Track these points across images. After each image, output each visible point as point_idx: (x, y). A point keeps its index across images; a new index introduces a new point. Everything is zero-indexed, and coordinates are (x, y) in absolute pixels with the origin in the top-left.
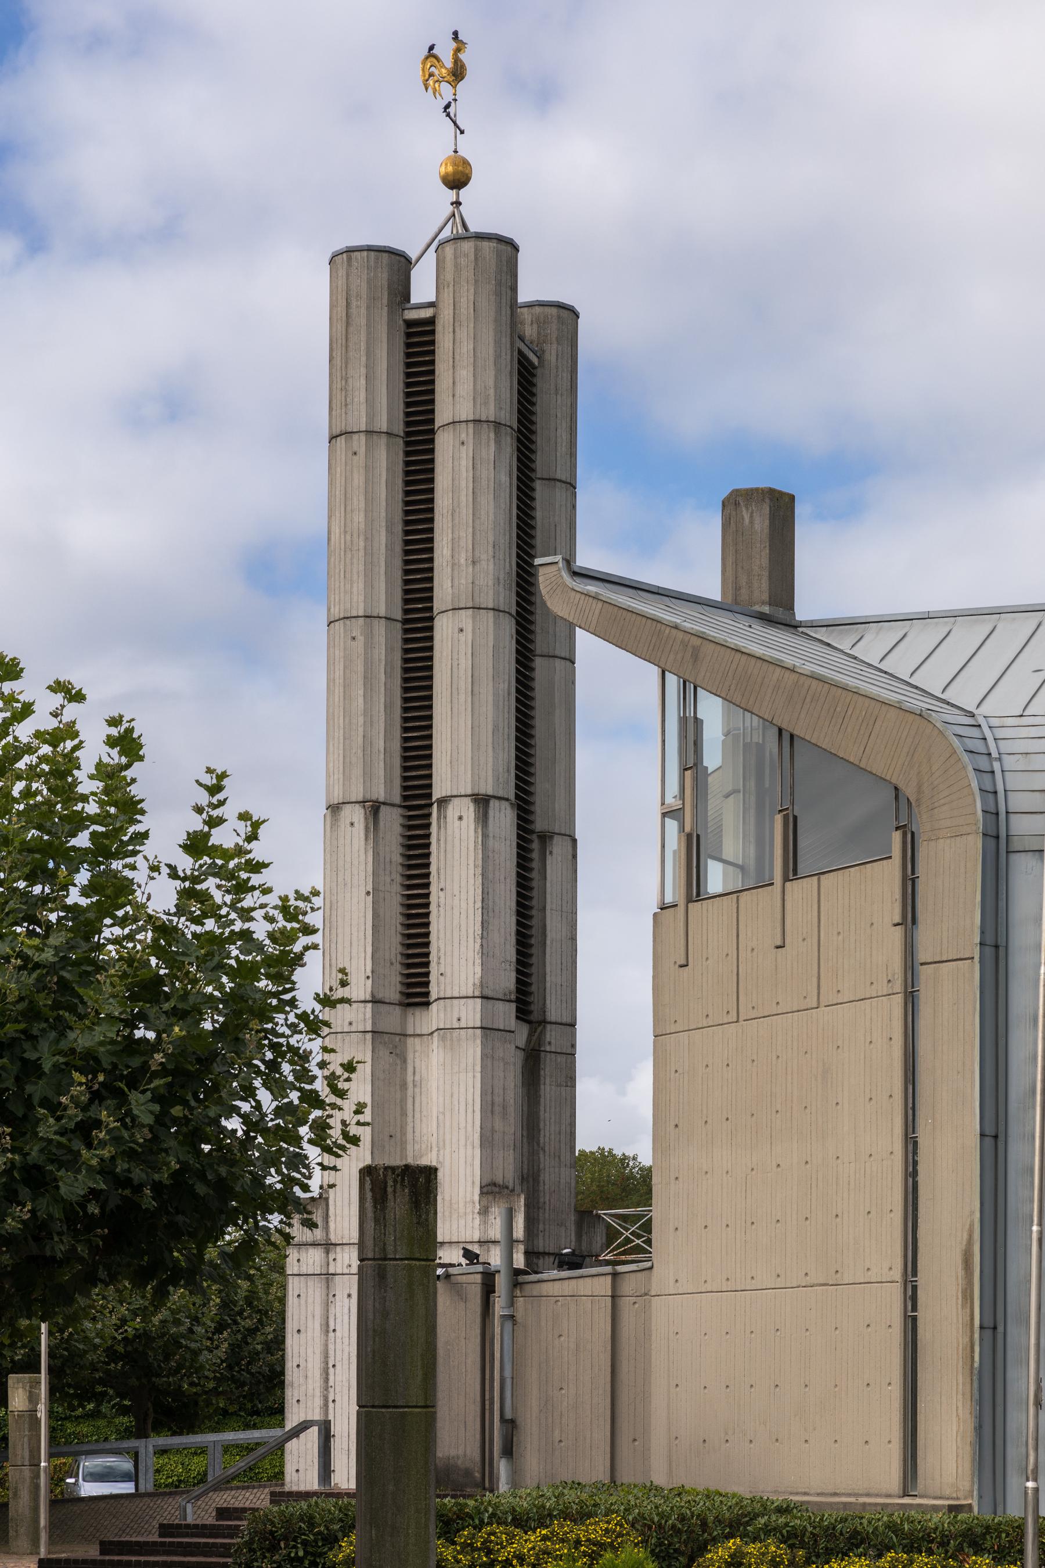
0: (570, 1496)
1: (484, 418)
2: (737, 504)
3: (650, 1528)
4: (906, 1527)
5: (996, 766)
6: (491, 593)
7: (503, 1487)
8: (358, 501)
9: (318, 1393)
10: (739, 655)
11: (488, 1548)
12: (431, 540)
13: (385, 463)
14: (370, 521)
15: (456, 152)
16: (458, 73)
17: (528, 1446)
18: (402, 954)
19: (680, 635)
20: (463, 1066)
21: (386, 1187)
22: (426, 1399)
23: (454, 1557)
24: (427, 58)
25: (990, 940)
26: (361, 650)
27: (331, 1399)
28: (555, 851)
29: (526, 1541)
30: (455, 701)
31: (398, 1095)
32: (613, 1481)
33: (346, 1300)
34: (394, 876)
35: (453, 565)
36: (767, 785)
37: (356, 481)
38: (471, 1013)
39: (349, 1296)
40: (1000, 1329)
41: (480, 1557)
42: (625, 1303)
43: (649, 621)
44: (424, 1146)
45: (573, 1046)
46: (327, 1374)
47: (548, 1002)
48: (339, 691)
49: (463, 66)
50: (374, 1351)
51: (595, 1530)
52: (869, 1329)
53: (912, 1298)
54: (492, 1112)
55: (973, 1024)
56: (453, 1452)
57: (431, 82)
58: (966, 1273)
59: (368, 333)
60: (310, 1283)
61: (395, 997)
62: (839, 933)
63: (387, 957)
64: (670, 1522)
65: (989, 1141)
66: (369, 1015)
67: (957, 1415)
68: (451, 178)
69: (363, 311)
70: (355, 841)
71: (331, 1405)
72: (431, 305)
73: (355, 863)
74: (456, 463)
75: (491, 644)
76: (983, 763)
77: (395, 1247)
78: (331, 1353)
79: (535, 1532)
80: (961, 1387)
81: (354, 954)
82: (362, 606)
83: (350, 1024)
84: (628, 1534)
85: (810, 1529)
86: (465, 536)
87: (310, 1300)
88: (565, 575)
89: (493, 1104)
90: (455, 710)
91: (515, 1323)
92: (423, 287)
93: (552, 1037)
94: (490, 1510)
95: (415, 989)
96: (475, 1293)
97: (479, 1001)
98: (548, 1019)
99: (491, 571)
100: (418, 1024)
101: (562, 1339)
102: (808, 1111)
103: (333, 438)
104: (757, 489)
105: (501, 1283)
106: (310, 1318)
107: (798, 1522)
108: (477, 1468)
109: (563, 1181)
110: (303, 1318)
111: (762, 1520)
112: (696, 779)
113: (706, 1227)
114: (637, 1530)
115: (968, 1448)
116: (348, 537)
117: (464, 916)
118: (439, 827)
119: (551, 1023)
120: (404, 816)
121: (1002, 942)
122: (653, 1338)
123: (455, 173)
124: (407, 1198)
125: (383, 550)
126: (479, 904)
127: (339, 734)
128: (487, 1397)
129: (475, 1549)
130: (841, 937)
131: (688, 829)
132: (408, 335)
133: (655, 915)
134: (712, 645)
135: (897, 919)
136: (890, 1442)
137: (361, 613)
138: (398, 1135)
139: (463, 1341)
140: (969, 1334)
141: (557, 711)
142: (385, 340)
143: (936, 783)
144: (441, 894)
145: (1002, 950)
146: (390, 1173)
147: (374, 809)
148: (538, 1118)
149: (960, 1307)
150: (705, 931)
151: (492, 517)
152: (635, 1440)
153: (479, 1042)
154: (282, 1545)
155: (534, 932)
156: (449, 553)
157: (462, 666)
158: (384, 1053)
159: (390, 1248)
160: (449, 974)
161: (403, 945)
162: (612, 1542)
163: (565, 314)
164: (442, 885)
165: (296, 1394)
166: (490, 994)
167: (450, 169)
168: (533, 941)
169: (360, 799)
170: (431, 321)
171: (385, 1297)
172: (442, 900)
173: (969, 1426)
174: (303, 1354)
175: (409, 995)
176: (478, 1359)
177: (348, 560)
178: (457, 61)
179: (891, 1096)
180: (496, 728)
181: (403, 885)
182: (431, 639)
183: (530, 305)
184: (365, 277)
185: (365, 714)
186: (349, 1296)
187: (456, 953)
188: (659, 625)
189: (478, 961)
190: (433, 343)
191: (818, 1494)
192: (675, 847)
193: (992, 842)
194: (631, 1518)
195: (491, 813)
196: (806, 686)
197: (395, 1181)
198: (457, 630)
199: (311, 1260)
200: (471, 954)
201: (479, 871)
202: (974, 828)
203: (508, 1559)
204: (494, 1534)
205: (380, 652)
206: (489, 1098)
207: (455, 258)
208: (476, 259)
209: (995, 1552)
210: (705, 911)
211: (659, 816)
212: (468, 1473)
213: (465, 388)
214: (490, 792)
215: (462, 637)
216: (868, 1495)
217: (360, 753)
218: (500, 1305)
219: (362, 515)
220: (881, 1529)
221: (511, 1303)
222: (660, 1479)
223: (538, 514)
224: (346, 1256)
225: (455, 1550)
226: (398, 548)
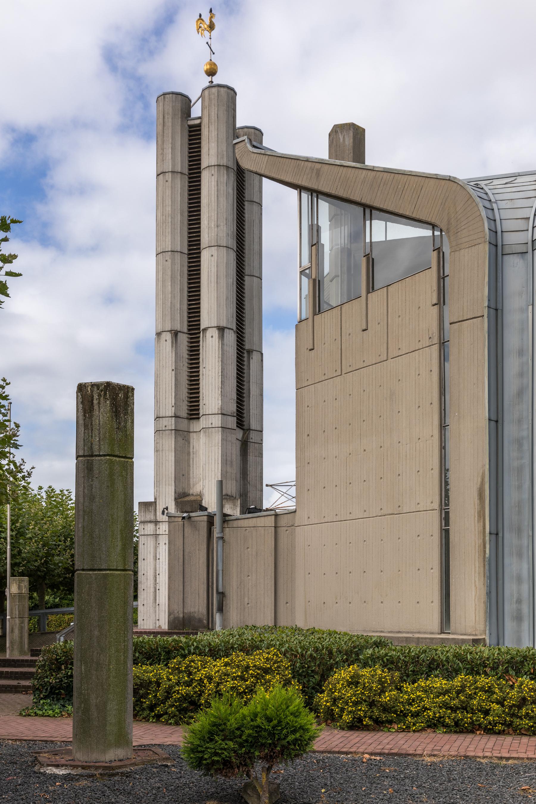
0: (248, 635)
1: (221, 164)
2: (336, 132)
3: (296, 656)
4: (469, 657)
5: (495, 206)
6: (225, 239)
7: (218, 628)
8: (168, 202)
9: (152, 586)
10: (342, 168)
11: (189, 671)
12: (200, 219)
13: (180, 185)
14: (173, 210)
15: (211, 60)
16: (211, 27)
17: (231, 606)
18: (188, 397)
19: (310, 164)
20: (213, 444)
21: (92, 400)
22: (125, 565)
23: (167, 677)
24: (199, 20)
25: (493, 306)
26: (170, 266)
27: (157, 589)
28: (254, 358)
29: (214, 666)
30: (210, 286)
31: (186, 458)
32: (275, 626)
33: (164, 546)
34: (184, 363)
35: (209, 227)
36: (352, 272)
37: (167, 193)
38: (217, 421)
39: (165, 544)
40: (500, 535)
41: (183, 678)
42: (281, 530)
43: (293, 160)
44: (197, 480)
45: (262, 440)
46: (156, 578)
47: (251, 421)
48: (160, 284)
49: (214, 24)
50: (83, 527)
51: (258, 659)
52: (419, 538)
53: (446, 518)
54: (226, 464)
55: (483, 355)
56: (192, 610)
57: (200, 30)
58: (480, 501)
59: (172, 129)
60: (149, 539)
61: (185, 415)
62: (399, 316)
63: (181, 398)
64: (309, 652)
65: (493, 423)
66: (173, 422)
67: (475, 586)
68: (209, 71)
69: (170, 120)
70: (167, 347)
71: (157, 591)
72: (200, 118)
73: (167, 357)
74: (210, 184)
75: (225, 262)
76: (488, 205)
77: (99, 446)
78: (158, 569)
79: (220, 659)
80: (477, 569)
81: (167, 396)
82: (170, 246)
83: (166, 426)
84: (281, 661)
85: (402, 658)
86: (214, 215)
87: (149, 546)
88: (249, 146)
89: (226, 460)
90: (210, 290)
91: (224, 541)
92: (196, 111)
93: (253, 436)
94: (195, 644)
95: (194, 412)
96: (204, 526)
97: (220, 415)
98: (251, 428)
99: (225, 231)
100: (195, 427)
101: (249, 549)
102: (382, 418)
103: (158, 175)
104: (346, 124)
105: (217, 520)
106: (149, 553)
107: (394, 653)
108: (205, 617)
109: (258, 497)
110: (146, 554)
111: (370, 651)
112: (317, 250)
113: (324, 487)
114: (287, 658)
115: (482, 605)
116: (164, 217)
117: (213, 379)
118: (203, 341)
119: (252, 430)
120: (188, 338)
121: (500, 307)
122: (297, 549)
123: (210, 69)
124: (108, 408)
125: (179, 223)
126: (220, 374)
127: (160, 302)
128: (210, 580)
129: (180, 672)
130: (400, 318)
131: (313, 277)
132: (190, 132)
133: (296, 325)
134: (327, 166)
135: (435, 301)
136: (432, 602)
137: (170, 250)
138: (187, 475)
139: (197, 552)
140: (482, 538)
141: (255, 299)
142: (180, 133)
143: (459, 217)
144: (204, 370)
145: (499, 311)
146: (95, 389)
147: (175, 334)
148: (247, 469)
149: (476, 522)
150: (323, 329)
151: (225, 207)
152: (287, 603)
153: (220, 433)
154: (63, 667)
155: (245, 391)
156: (207, 222)
157: (213, 271)
158: (180, 439)
159: (96, 447)
160: (207, 404)
161: (188, 393)
162: (271, 667)
163: (257, 132)
164: (204, 366)
165: (143, 586)
166: (225, 413)
167: (208, 67)
168: (244, 395)
169: (169, 329)
170: (199, 125)
171: (92, 485)
172: (204, 373)
173: (483, 592)
174: (145, 569)
175: (191, 415)
176: (205, 561)
177: (164, 228)
178: (211, 22)
179: (431, 403)
180: (227, 298)
181: (188, 367)
182: (200, 261)
183: (242, 128)
184: (171, 105)
185: (171, 293)
186: (165, 544)
187: (210, 395)
188: (298, 161)
189: (220, 398)
190: (200, 134)
191: (389, 632)
192: (307, 293)
193: (494, 248)
194: (283, 650)
195: (225, 335)
196: (380, 178)
197: (99, 395)
198: (210, 256)
199: (150, 528)
200: (217, 395)
201: (220, 359)
202: (483, 240)
203: (201, 679)
204: (193, 661)
205: (178, 267)
206: (225, 457)
207: (209, 95)
208: (218, 95)
209: (531, 674)
210: (323, 319)
211: (299, 273)
212: (200, 620)
213: (213, 151)
214: (225, 326)
215: (213, 258)
216: (419, 633)
217: (169, 310)
218: (216, 533)
219: (170, 207)
220: (451, 657)
221: (222, 530)
222: (300, 624)
223: (246, 216)
224: (164, 527)
225: (168, 672)
226: (186, 222)
